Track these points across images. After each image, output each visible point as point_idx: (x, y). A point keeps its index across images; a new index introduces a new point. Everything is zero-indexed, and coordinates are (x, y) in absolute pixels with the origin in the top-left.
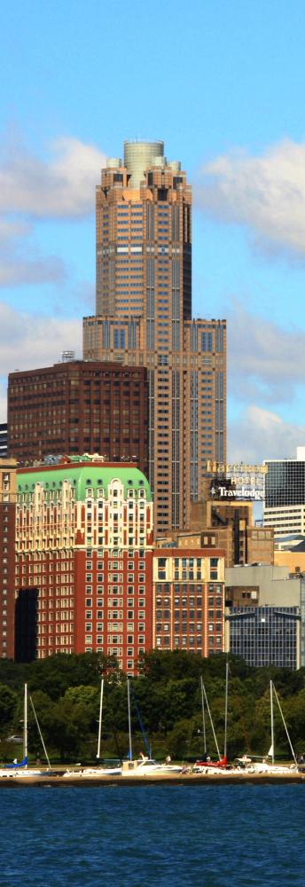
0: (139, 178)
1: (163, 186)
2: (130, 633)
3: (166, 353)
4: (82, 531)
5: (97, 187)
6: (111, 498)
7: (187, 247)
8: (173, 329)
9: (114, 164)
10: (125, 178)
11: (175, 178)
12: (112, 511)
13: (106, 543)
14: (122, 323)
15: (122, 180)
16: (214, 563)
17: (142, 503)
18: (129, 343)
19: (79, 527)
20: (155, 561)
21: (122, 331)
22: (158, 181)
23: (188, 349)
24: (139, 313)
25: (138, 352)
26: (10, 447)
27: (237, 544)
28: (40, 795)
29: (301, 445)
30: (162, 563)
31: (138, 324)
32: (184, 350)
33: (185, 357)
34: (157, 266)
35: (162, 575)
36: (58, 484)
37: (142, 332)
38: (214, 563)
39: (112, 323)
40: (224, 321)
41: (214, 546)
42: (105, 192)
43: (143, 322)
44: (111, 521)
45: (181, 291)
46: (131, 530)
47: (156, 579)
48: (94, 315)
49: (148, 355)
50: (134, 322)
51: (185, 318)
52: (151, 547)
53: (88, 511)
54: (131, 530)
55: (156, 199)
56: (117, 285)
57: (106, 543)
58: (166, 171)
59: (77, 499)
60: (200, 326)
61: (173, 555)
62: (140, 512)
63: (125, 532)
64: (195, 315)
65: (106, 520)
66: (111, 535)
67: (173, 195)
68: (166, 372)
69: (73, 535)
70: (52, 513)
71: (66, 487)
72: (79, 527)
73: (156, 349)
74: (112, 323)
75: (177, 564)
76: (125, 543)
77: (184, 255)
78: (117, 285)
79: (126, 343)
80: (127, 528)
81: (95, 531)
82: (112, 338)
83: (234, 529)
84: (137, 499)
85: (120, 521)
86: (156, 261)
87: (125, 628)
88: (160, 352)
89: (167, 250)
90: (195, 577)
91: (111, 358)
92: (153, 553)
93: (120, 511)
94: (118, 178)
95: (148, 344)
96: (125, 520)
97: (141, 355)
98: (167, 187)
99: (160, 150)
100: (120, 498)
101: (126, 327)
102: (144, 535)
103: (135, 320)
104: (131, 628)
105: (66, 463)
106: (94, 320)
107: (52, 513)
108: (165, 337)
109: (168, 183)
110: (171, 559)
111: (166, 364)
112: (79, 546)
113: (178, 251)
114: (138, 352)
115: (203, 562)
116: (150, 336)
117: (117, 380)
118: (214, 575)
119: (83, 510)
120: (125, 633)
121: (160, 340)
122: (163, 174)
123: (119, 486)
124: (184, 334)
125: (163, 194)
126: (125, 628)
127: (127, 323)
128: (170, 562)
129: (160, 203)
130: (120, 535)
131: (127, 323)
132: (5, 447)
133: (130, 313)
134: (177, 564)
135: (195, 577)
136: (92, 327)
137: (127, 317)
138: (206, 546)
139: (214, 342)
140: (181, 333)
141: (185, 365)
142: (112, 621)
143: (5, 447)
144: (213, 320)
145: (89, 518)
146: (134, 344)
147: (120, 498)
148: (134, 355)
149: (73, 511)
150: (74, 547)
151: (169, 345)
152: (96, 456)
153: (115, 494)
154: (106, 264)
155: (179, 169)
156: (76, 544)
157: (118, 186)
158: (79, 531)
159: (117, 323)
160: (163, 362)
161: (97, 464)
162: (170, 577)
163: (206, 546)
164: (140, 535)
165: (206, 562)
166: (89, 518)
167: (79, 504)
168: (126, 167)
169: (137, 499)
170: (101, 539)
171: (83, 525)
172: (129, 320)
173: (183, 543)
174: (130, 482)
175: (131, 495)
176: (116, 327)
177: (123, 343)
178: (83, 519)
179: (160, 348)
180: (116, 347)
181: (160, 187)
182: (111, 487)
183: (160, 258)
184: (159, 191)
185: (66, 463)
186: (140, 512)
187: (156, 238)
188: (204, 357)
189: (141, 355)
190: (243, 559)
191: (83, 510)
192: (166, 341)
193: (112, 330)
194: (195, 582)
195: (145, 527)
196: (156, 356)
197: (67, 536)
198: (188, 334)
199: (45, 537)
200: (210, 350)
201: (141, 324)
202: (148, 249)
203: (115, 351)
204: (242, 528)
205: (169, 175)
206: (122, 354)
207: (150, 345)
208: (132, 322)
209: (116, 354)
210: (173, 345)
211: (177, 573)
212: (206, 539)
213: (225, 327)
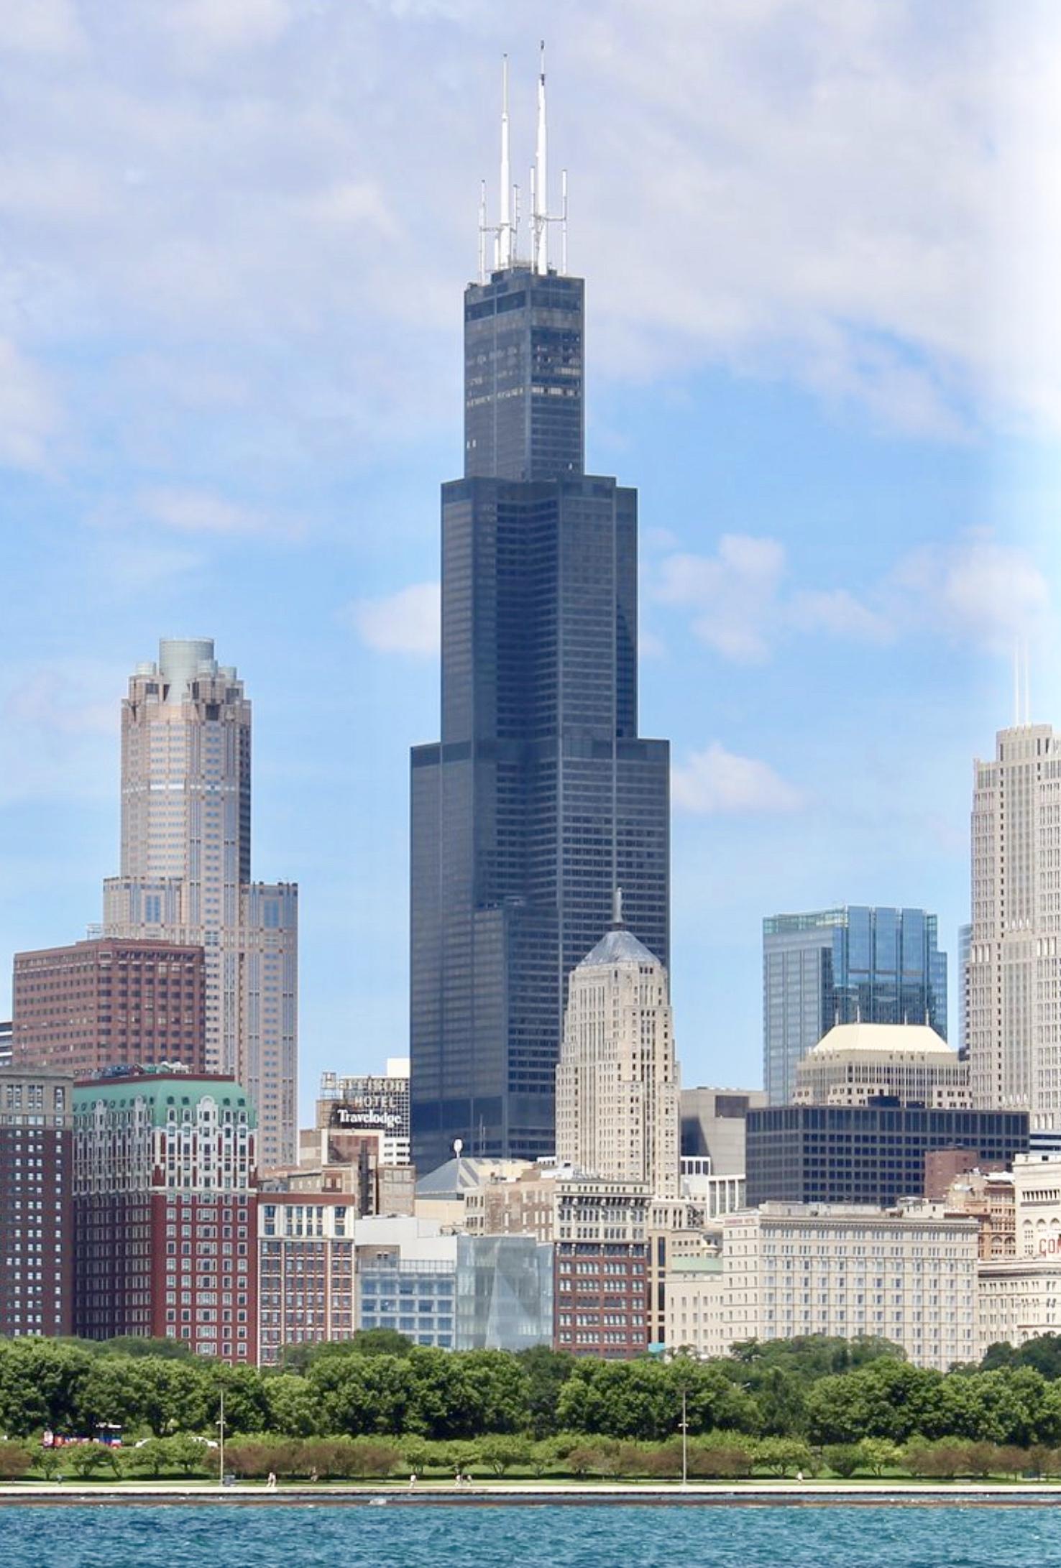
0: (179, 690)
1: (213, 700)
2: (186, 1307)
3: (217, 928)
4: (162, 1167)
5: (123, 701)
6: (200, 1122)
7: (245, 782)
8: (226, 896)
9: (145, 670)
10: (161, 689)
11: (228, 690)
12: (202, 1141)
13: (195, 1185)
14: (157, 887)
15: (157, 692)
16: (340, 1213)
17: (244, 1130)
18: (166, 914)
19: (158, 1161)
20: (261, 1209)
21: (157, 898)
22: (205, 693)
23: (246, 923)
24: (180, 874)
25: (178, 927)
26: (16, 1053)
27: (365, 1186)
28: (464, 1560)
29: (397, 1056)
30: (270, 1213)
31: (179, 888)
32: (241, 924)
33: (242, 934)
34: (205, 809)
35: (270, 1229)
36: (89, 1106)
37: (184, 899)
38: (340, 1213)
39: (143, 887)
40: (295, 885)
41: (340, 1190)
42: (134, 708)
43: (185, 887)
44: (201, 1155)
45: (238, 844)
46: (228, 1167)
47: (261, 1233)
48: (119, 875)
49: (191, 932)
50: (175, 886)
51: (242, 881)
52: (255, 1190)
53: (169, 1140)
54: (228, 1167)
55: (204, 718)
56: (149, 836)
57: (195, 1185)
58: (218, 680)
59: (154, 1124)
60: (262, 892)
61: (284, 1202)
62: (241, 1142)
63: (220, 1169)
64: (255, 878)
65: (195, 1153)
66: (201, 1174)
67: (226, 713)
68: (216, 955)
69: (149, 1173)
70: (119, 1143)
71: (139, 1107)
72: (158, 1161)
73: (202, 923)
74: (143, 887)
75: (289, 1214)
76: (220, 1185)
77: (241, 795)
78: (149, 836)
79: (163, 914)
80: (222, 1164)
81: (220, 1169)
82: (143, 908)
83: (360, 1168)
84: (235, 1124)
85: (214, 1155)
86: (203, 803)
87: (220, 1301)
88: (208, 928)
89: (217, 788)
90: (314, 1231)
91: (141, 935)
92: (257, 1199)
93: (212, 1140)
94: (151, 688)
95: (191, 915)
96: (220, 1153)
97: (183, 931)
98: (218, 702)
99: (208, 650)
100: (212, 1123)
101: (163, 892)
102: (245, 1174)
103: (174, 883)
104: (227, 1301)
105: (137, 1074)
106: (118, 882)
107: (119, 1143)
108: (216, 907)
109: (220, 696)
110: (282, 1207)
111: (216, 944)
112: (158, 1188)
113: (233, 789)
114: (178, 927)
115: (324, 1211)
116: (195, 906)
117: (124, 962)
118: (340, 1230)
119: (163, 1139)
120: (219, 1307)
121: (209, 911)
122: (213, 683)
123: (210, 1106)
124: (241, 902)
125: (213, 711)
126: (220, 1301)
127: (163, 887)
128: (281, 1210)
129: (209, 723)
130: (213, 1174)
131: (163, 887)
132: (10, 1054)
133: (167, 874)
134: (289, 1214)
135: (314, 1231)
136: (116, 893)
137: (163, 879)
138: (329, 1190)
139: (163, 909)
140: (237, 902)
141: (241, 945)
142: (202, 1290)
143: (10, 1054)
144: (280, 884)
145: (172, 1150)
146: (173, 916)
147: (212, 1123)
148: (173, 931)
149: (149, 1140)
150: (151, 1189)
151: (221, 917)
152: (177, 1066)
153: (207, 1118)
154: (134, 806)
155: (235, 676)
156: (154, 1184)
157: (151, 700)
158: (157, 1167)
159: (149, 887)
160: (212, 941)
161: (180, 1076)
162: (280, 1232)
163: (329, 1190)
164: (240, 1174)
165: (329, 1212)
166: (172, 1150)
167: (158, 1132)
168: (162, 674)
169: (235, 1124)
170: (187, 1181)
171: (163, 1160)
172: (166, 883)
173: (297, 1185)
174: (227, 1102)
175: (228, 1120)
176: (149, 893)
177: (157, 915)
178: (163, 1151)
179: (208, 922)
180: (149, 920)
181: (209, 702)
182: (201, 1108)
183: (208, 798)
184: (208, 707)
185: (137, 1074)
186: (241, 1142)
187: (203, 772)
188: (267, 934)
189: (183, 931)
190: (372, 1208)
191: (163, 1139)
192: (216, 912)
193: (143, 897)
194: (315, 1238)
195: (247, 1163)
196: (203, 932)
197: (141, 1174)
198: (246, 902)
199: (110, 1176)
200: (157, 920)
201: (183, 889)
202: (193, 787)
203: (147, 925)
204: (372, 1166)
205: (222, 685)
206: (157, 930)
207: (195, 917)
208: (136, 885)
209: (148, 929)
210: (226, 917)
211: (290, 1226)
212: (329, 1181)
213: (296, 893)
